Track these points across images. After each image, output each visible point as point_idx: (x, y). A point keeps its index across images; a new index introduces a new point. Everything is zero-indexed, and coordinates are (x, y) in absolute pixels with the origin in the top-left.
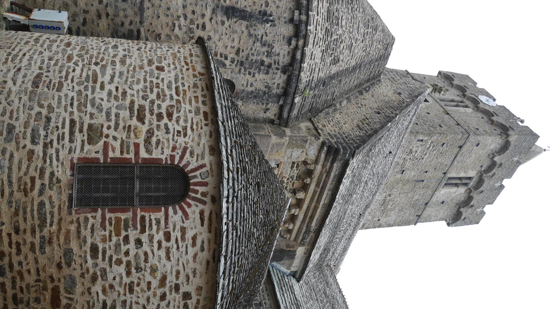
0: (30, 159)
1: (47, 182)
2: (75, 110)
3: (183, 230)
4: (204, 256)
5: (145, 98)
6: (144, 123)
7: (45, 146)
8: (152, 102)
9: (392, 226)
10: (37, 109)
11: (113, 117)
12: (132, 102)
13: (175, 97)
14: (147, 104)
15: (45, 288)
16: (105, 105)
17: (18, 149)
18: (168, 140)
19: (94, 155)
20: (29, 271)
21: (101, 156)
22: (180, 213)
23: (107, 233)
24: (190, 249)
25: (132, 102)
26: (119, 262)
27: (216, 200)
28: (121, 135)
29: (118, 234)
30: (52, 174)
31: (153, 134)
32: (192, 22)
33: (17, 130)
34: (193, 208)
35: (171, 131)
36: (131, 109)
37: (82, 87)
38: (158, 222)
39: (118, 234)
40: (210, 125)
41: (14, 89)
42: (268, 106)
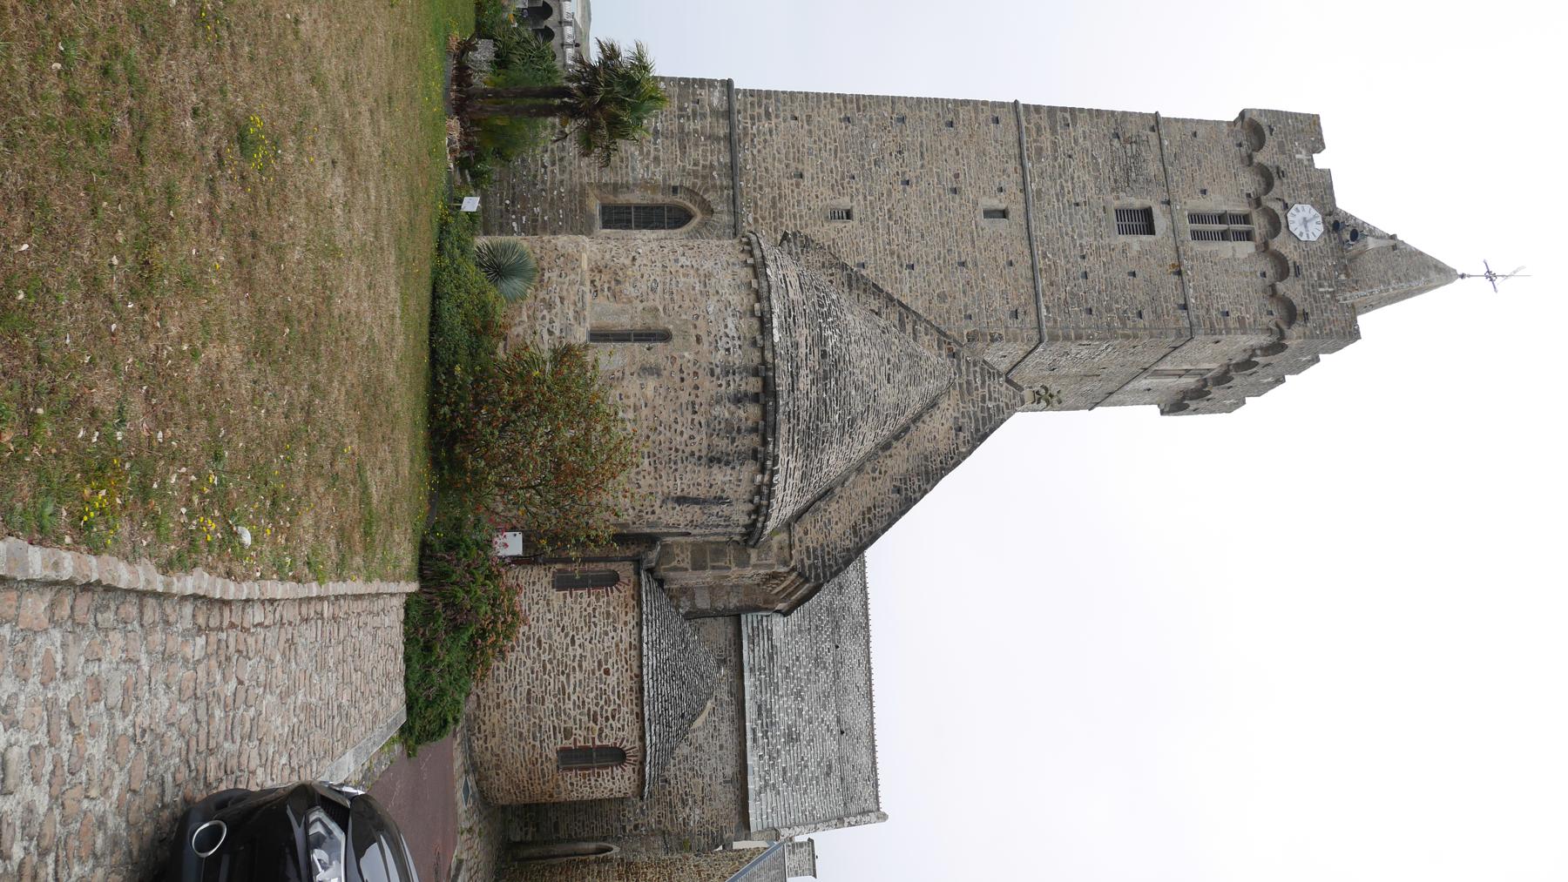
0: (534, 749)
5: (597, 705)
7: (541, 742)
8: (602, 708)
10: (533, 720)
12: (589, 709)
14: (598, 710)
16: (573, 713)
19: (568, 745)
25: (589, 709)
27: (642, 763)
36: (589, 715)
41: (517, 706)
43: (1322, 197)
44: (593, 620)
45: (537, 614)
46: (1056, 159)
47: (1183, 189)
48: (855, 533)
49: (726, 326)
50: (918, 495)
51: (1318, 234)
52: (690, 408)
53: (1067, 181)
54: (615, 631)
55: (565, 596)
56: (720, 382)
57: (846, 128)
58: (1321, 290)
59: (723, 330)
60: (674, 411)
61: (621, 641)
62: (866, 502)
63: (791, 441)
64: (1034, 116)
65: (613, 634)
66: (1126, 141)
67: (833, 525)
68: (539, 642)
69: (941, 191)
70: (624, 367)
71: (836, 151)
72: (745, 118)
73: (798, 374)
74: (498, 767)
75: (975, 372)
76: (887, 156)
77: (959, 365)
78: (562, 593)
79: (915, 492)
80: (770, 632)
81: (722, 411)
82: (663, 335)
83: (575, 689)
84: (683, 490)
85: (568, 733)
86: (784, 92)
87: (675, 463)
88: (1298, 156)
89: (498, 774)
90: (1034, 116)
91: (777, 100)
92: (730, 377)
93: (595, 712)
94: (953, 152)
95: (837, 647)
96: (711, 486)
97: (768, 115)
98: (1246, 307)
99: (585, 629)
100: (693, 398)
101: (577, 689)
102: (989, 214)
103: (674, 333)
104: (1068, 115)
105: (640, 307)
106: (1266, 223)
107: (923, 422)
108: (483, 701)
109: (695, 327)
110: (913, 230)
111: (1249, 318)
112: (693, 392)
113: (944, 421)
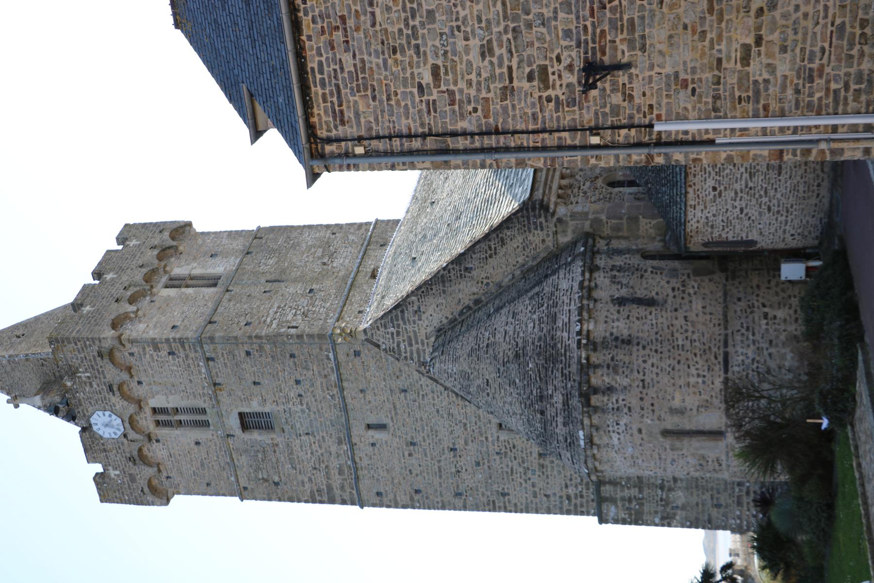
9: (304, 226)
32: (684, 292)
43: (93, 443)
46: (327, 467)
47: (216, 445)
48: (502, 240)
49: (619, 439)
50: (451, 267)
51: (95, 416)
52: (646, 384)
53: (317, 451)
54: (707, 218)
55: (747, 237)
57: (503, 489)
58: (88, 374)
59: (622, 437)
60: (658, 382)
62: (492, 262)
64: (346, 496)
66: (266, 480)
67: (521, 246)
68: (769, 209)
69: (423, 444)
72: (588, 496)
73: (564, 405)
75: (406, 352)
76: (470, 470)
77: (419, 357)
78: (750, 238)
79: (453, 269)
81: (621, 381)
84: (651, 313)
87: (657, 340)
88: (118, 472)
90: (346, 496)
92: (616, 406)
94: (414, 472)
96: (628, 317)
97: (569, 498)
98: (153, 359)
100: (644, 391)
101: (739, 176)
102: (382, 427)
103: (659, 436)
104: (318, 498)
105: (684, 451)
106: (140, 422)
107: (447, 318)
109: (642, 439)
110: (445, 416)
111: (150, 350)
112: (644, 396)
113: (431, 318)
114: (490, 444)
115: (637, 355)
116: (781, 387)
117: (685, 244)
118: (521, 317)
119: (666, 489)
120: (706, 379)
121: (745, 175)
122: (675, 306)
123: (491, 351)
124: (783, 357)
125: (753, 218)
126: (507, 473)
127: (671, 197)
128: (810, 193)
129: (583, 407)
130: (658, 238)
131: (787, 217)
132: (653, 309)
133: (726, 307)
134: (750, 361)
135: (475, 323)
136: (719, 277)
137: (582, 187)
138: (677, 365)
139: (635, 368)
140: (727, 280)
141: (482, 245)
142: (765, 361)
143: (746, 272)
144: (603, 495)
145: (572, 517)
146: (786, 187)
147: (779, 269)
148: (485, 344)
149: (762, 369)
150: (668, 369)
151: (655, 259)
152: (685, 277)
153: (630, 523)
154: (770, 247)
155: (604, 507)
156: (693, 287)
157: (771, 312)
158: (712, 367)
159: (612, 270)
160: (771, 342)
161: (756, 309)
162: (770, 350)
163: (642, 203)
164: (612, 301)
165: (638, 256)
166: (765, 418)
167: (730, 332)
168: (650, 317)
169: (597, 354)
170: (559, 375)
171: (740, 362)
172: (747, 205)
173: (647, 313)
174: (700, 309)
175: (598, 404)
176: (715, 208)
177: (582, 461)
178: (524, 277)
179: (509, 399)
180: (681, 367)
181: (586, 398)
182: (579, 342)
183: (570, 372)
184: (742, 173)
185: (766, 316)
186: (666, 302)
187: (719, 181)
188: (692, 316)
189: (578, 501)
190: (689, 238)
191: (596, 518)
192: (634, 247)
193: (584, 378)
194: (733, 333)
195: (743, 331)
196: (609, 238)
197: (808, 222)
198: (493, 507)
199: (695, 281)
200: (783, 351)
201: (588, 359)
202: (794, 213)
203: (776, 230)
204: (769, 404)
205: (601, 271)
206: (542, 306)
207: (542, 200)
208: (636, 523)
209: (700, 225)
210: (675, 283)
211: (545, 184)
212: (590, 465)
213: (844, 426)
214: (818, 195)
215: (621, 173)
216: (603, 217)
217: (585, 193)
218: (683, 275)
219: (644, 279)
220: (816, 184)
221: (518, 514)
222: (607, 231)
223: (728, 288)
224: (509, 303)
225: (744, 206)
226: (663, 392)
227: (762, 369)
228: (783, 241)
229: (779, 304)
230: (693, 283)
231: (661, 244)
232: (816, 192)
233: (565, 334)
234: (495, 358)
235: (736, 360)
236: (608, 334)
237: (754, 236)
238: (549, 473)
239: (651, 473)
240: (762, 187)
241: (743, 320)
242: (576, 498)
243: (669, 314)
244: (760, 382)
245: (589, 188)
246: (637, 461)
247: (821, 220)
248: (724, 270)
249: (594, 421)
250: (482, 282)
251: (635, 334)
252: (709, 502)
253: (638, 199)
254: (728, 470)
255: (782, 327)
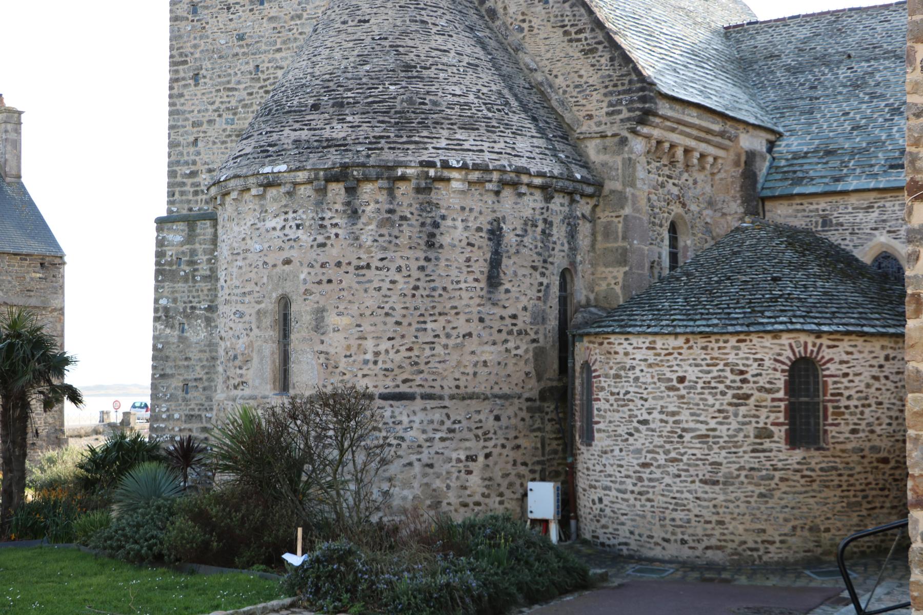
0: (787, 480)
1: (805, 467)
2: (741, 450)
3: (842, 362)
4: (860, 342)
5: (723, 394)
6: (752, 395)
7: (775, 470)
8: (728, 387)
11: (747, 419)
12: (730, 404)
13: (721, 367)
14: (730, 393)
15: (877, 468)
16: (734, 426)
17: (779, 489)
18: (768, 374)
19: (783, 434)
20: (866, 478)
21: (784, 428)
22: (828, 365)
23: (843, 422)
24: (855, 357)
25: (730, 404)
26: (862, 413)
28: (763, 413)
29: (843, 414)
30: (798, 463)
31: (762, 387)
32: (510, 333)
33: (763, 491)
34: (825, 354)
35: (759, 371)
36: (737, 405)
37: (714, 446)
38: (835, 383)
39: (843, 414)
40: (750, 337)
42: (580, 215)
44: (621, 396)
45: (615, 467)
48: (593, 51)
49: (274, 229)
54: (633, 368)
55: (599, 431)
56: (333, 236)
57: (204, 77)
59: (278, 233)
60: (366, 291)
61: (646, 360)
63: (406, 146)
65: (637, 371)
68: (645, 465)
70: (313, 352)
71: (230, 89)
73: (327, 140)
74: (814, 529)
76: (232, 25)
78: (596, 435)
80: (796, 156)
82: (282, 305)
83: (702, 422)
84: (476, 280)
85: (764, 434)
86: (170, 156)
87: (434, 289)
89: (827, 530)
91: (178, 163)
93: (734, 396)
95: (849, 56)
97: (193, 174)
99: (631, 404)
100: (351, 269)
101: (702, 418)
103: (280, 292)
105: (256, 331)
108: (713, 542)
109: (275, 266)
112: (344, 268)
114: (270, 56)
115: (413, 258)
116: (359, 481)
117: (588, 334)
118: (470, 77)
119: (209, 315)
120: (371, 365)
121: (703, 427)
122: (487, 318)
123: (414, 27)
124: (407, 484)
125: (631, 440)
126: (229, 82)
127: (667, 312)
128: (670, 529)
129: (325, 170)
130: (592, 296)
131: (632, 492)
132: (483, 284)
133: (486, 398)
134: (401, 434)
135: (460, 7)
136: (533, 388)
137: (671, 181)
138: (394, 320)
139: (389, 255)
140: (528, 400)
141: (585, 18)
142: (400, 457)
143: (539, 429)
144: (199, 223)
145: (164, 180)
146: (682, 492)
147: (543, 479)
148: (426, 18)
149: (389, 452)
150: (387, 306)
151: (560, 291)
152: (533, 336)
153: (158, 263)
154: (580, 466)
155: (182, 226)
156: (517, 348)
157: (476, 467)
158: (391, 375)
159: (545, 221)
160: (431, 466)
161: (482, 443)
162: (417, 465)
163: (646, 271)
164: (497, 220)
165: (565, 264)
166: (308, 455)
167: (447, 403)
168: (470, 278)
169: (412, 194)
170: (378, 132)
171: (399, 418)
172: (653, 430)
173: (478, 275)
174: (483, 359)
175: (330, 195)
176: (649, 380)
177: (238, 171)
178: (532, 87)
179: (337, 55)
180: (391, 326)
181: (340, 175)
182: (432, 164)
183: (382, 149)
184: (707, 423)
185: (471, 458)
186: (495, 304)
187: (694, 388)
188: (472, 344)
189: (188, 188)
190: (599, 340)
191: (164, 214)
192: (579, 258)
193: (373, 172)
194: (445, 407)
195: (448, 424)
196: (593, 220)
197: (623, 524)
198: (177, 61)
199: (526, 351)
200: (416, 484)
201: (403, 178)
202: (638, 504)
203: (610, 476)
204: (331, 462)
205: (543, 204)
206: (489, 110)
207: (656, 115)
208: (158, 272)
209: (620, 358)
210: (524, 319)
211: (679, 122)
212: (232, 184)
213: (290, 592)
214: (667, 540)
215: (689, 242)
216: (627, 211)
217: (662, 186)
218: (536, 333)
219: (532, 271)
220: (686, 537)
221: (167, 100)
222: (604, 216)
223: (516, 401)
224: (491, 61)
225: (652, 426)
226: (350, 298)
227: (389, 452)
228: (591, 486)
229: (490, 479)
230: (524, 347)
231: (583, 302)
232: (673, 538)
233: (443, 143)
234: (405, 33)
235: (401, 412)
236: (443, 212)
237: (601, 441)
238: (229, 145)
239: (222, 282)
240: (682, 455)
241: (465, 423)
242: (193, 185)
243: (475, 310)
244: (367, 448)
245: (669, 193)
246: (240, 258)
247: (626, 544)
248: (543, 395)
249: (302, 187)
250: (524, 21)
251: (444, 254)
252: (191, 376)
253: (652, 267)
254: (228, 399)
255: (454, 484)
